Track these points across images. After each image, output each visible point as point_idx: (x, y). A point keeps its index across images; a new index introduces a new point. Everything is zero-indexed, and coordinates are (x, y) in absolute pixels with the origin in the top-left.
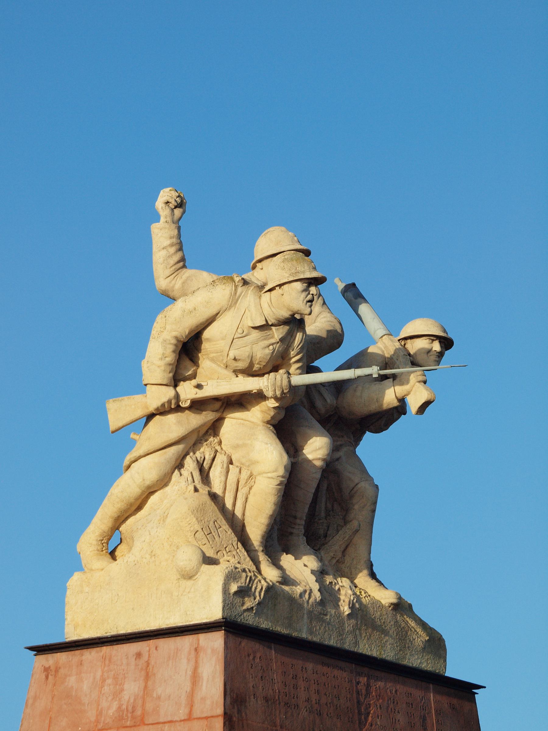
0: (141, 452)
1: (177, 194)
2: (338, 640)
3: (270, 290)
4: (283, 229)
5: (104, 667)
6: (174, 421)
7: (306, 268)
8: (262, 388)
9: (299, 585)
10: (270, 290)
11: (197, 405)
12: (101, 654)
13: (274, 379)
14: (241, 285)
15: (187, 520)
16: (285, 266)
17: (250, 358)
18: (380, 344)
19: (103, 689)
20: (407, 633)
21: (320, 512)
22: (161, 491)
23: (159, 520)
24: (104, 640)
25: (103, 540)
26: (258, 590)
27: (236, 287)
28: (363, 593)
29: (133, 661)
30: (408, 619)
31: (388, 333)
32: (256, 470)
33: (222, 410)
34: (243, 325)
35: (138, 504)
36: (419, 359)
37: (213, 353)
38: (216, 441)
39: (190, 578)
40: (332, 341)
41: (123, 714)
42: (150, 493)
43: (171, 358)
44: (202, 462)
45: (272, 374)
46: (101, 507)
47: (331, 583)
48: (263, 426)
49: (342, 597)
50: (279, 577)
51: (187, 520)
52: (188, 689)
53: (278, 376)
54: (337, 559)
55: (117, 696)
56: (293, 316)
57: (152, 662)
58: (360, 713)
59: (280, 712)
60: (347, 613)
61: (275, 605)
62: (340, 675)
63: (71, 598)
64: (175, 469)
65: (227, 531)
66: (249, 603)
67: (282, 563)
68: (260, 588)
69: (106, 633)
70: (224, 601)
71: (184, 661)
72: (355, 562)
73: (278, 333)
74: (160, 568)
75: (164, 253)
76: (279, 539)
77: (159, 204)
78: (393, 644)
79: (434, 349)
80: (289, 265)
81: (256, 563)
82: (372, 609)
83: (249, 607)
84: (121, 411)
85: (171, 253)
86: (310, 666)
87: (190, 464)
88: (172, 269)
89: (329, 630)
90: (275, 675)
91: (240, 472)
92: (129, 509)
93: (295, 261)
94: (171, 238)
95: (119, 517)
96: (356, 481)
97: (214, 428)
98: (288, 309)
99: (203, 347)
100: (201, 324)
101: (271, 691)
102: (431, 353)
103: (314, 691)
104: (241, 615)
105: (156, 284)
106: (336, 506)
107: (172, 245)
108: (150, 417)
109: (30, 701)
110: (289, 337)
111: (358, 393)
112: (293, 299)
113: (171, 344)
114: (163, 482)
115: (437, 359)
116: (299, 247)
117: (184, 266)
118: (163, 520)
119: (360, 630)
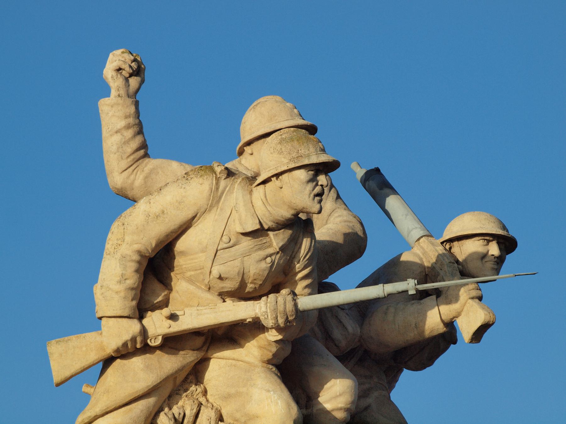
0: (98, 410)
1: (132, 58)
3: (264, 182)
4: (278, 98)
6: (142, 366)
7: (312, 149)
8: (259, 315)
10: (264, 182)
11: (172, 343)
13: (274, 303)
14: (224, 177)
16: (283, 150)
17: (241, 275)
18: (416, 250)
27: (218, 179)
31: (427, 233)
33: (205, 348)
34: (229, 231)
36: (472, 267)
37: (190, 270)
40: (352, 247)
43: (133, 280)
44: (181, 420)
45: (272, 296)
48: (263, 367)
53: (279, 298)
56: (296, 215)
73: (277, 240)
75: (117, 138)
77: (109, 72)
79: (491, 253)
84: (67, 356)
85: (127, 138)
88: (129, 160)
93: (296, 142)
94: (126, 117)
97: (196, 373)
98: (290, 207)
99: (176, 263)
100: (172, 232)
105: (109, 180)
107: (128, 127)
108: (108, 362)
111: (390, 317)
112: (295, 192)
113: (132, 261)
115: (496, 267)
116: (301, 122)
117: (146, 155)
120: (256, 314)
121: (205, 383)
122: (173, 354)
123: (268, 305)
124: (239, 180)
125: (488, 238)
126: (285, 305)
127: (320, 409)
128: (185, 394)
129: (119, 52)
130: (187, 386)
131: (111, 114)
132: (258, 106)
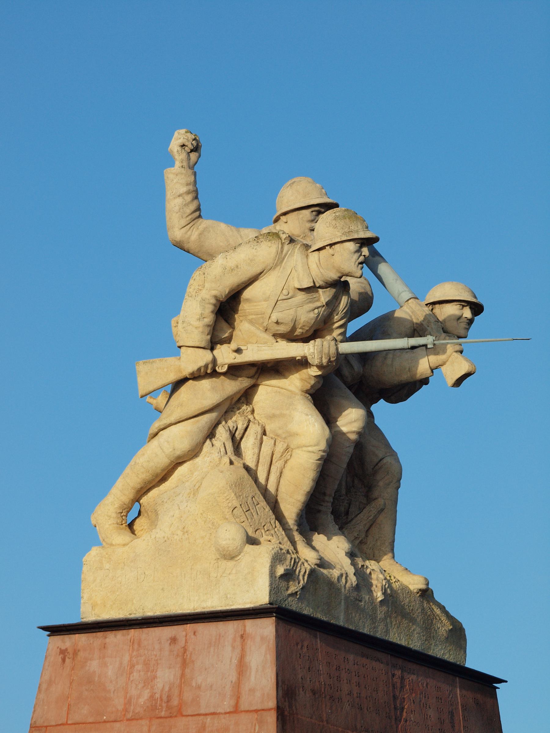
0: (172, 419)
1: (194, 137)
2: (371, 628)
4: (310, 179)
5: (133, 652)
6: (209, 387)
7: (360, 227)
8: (307, 355)
9: (335, 568)
10: (319, 250)
11: (234, 370)
12: (129, 637)
13: (320, 346)
14: (287, 243)
15: (225, 495)
16: (338, 225)
17: (293, 322)
19: (131, 676)
20: (432, 621)
21: (352, 490)
22: (191, 462)
23: (189, 493)
24: (133, 622)
25: (122, 513)
26: (302, 573)
28: (392, 578)
29: (167, 646)
30: (433, 607)
32: (294, 443)
33: (256, 377)
34: (289, 286)
35: (163, 476)
36: (450, 326)
37: (252, 314)
38: (249, 409)
39: (232, 558)
41: (156, 703)
42: (177, 463)
43: (209, 319)
44: (234, 432)
46: (121, 477)
47: (363, 566)
48: (301, 395)
49: (374, 582)
50: (317, 559)
51: (225, 495)
52: (234, 679)
53: (325, 343)
54: (360, 539)
55: (148, 684)
57: (190, 649)
58: (395, 708)
59: (326, 706)
60: (380, 599)
61: (316, 589)
62: (377, 668)
63: (88, 573)
64: (207, 439)
65: (265, 508)
66: (294, 588)
67: (314, 543)
68: (304, 571)
69: (130, 614)
70: (271, 585)
71: (229, 649)
72: (379, 543)
73: (324, 296)
74: (196, 545)
75: (179, 201)
76: (312, 519)
77: (174, 146)
78: (419, 634)
79: (464, 316)
80: (342, 223)
81: (293, 543)
82: (401, 595)
83: (294, 592)
84: (153, 374)
85: (187, 201)
86: (351, 657)
87: (222, 433)
88: (188, 219)
89: (363, 617)
90: (321, 666)
91: (275, 444)
92: (153, 480)
93: (348, 220)
94: (188, 184)
95: (142, 488)
96: (381, 456)
97: (246, 396)
98: (338, 271)
100: (243, 283)
101: (317, 683)
102: (461, 320)
103: (355, 683)
104: (286, 600)
105: (169, 234)
106: (356, 481)
107: (188, 193)
109: (44, 686)
110: (335, 300)
113: (210, 303)
114: (194, 452)
115: (467, 327)
117: (200, 216)
118: (194, 494)
119: (390, 617)
120: (305, 353)
121: (253, 404)
122: (234, 380)
123: (316, 347)
124: (299, 246)
125: (463, 304)
126: (329, 348)
127: (337, 431)
128: (238, 412)
129: (183, 131)
130: (240, 405)
131: (175, 181)
132: (294, 184)
